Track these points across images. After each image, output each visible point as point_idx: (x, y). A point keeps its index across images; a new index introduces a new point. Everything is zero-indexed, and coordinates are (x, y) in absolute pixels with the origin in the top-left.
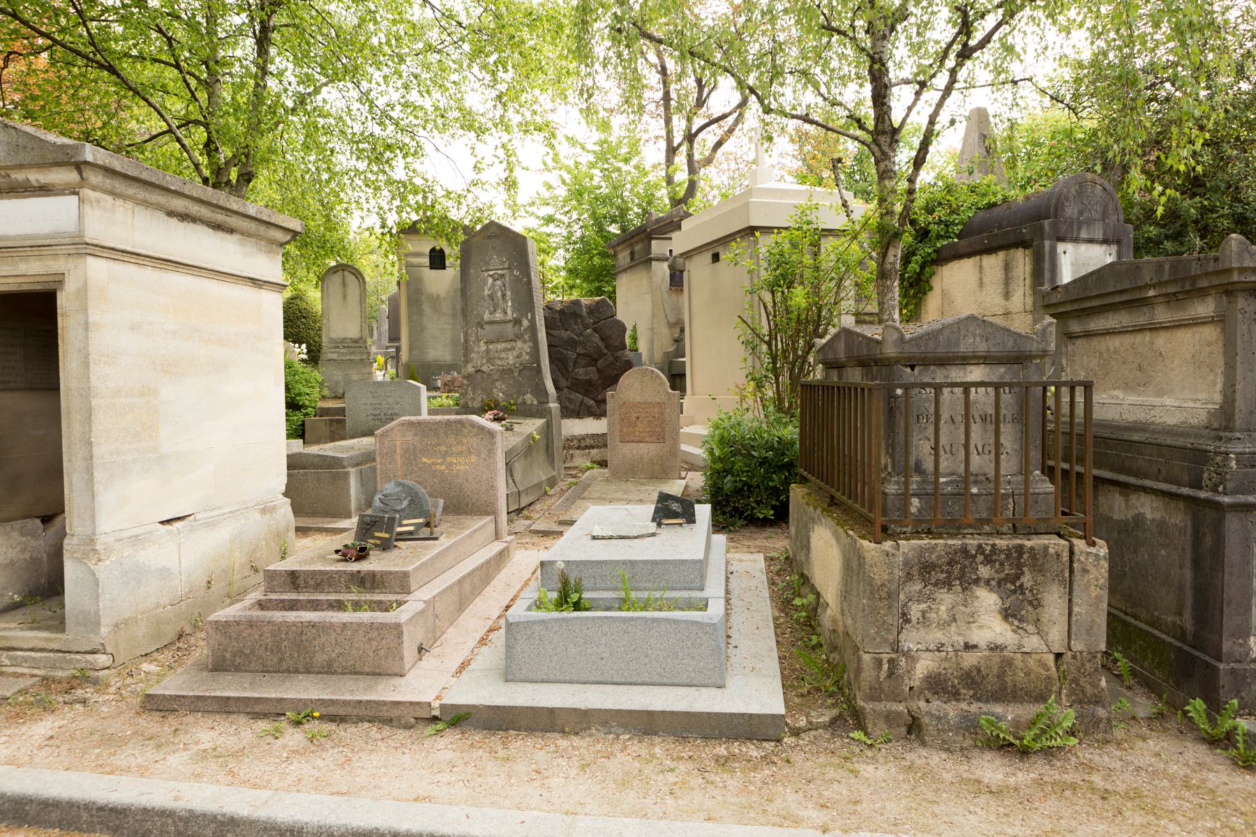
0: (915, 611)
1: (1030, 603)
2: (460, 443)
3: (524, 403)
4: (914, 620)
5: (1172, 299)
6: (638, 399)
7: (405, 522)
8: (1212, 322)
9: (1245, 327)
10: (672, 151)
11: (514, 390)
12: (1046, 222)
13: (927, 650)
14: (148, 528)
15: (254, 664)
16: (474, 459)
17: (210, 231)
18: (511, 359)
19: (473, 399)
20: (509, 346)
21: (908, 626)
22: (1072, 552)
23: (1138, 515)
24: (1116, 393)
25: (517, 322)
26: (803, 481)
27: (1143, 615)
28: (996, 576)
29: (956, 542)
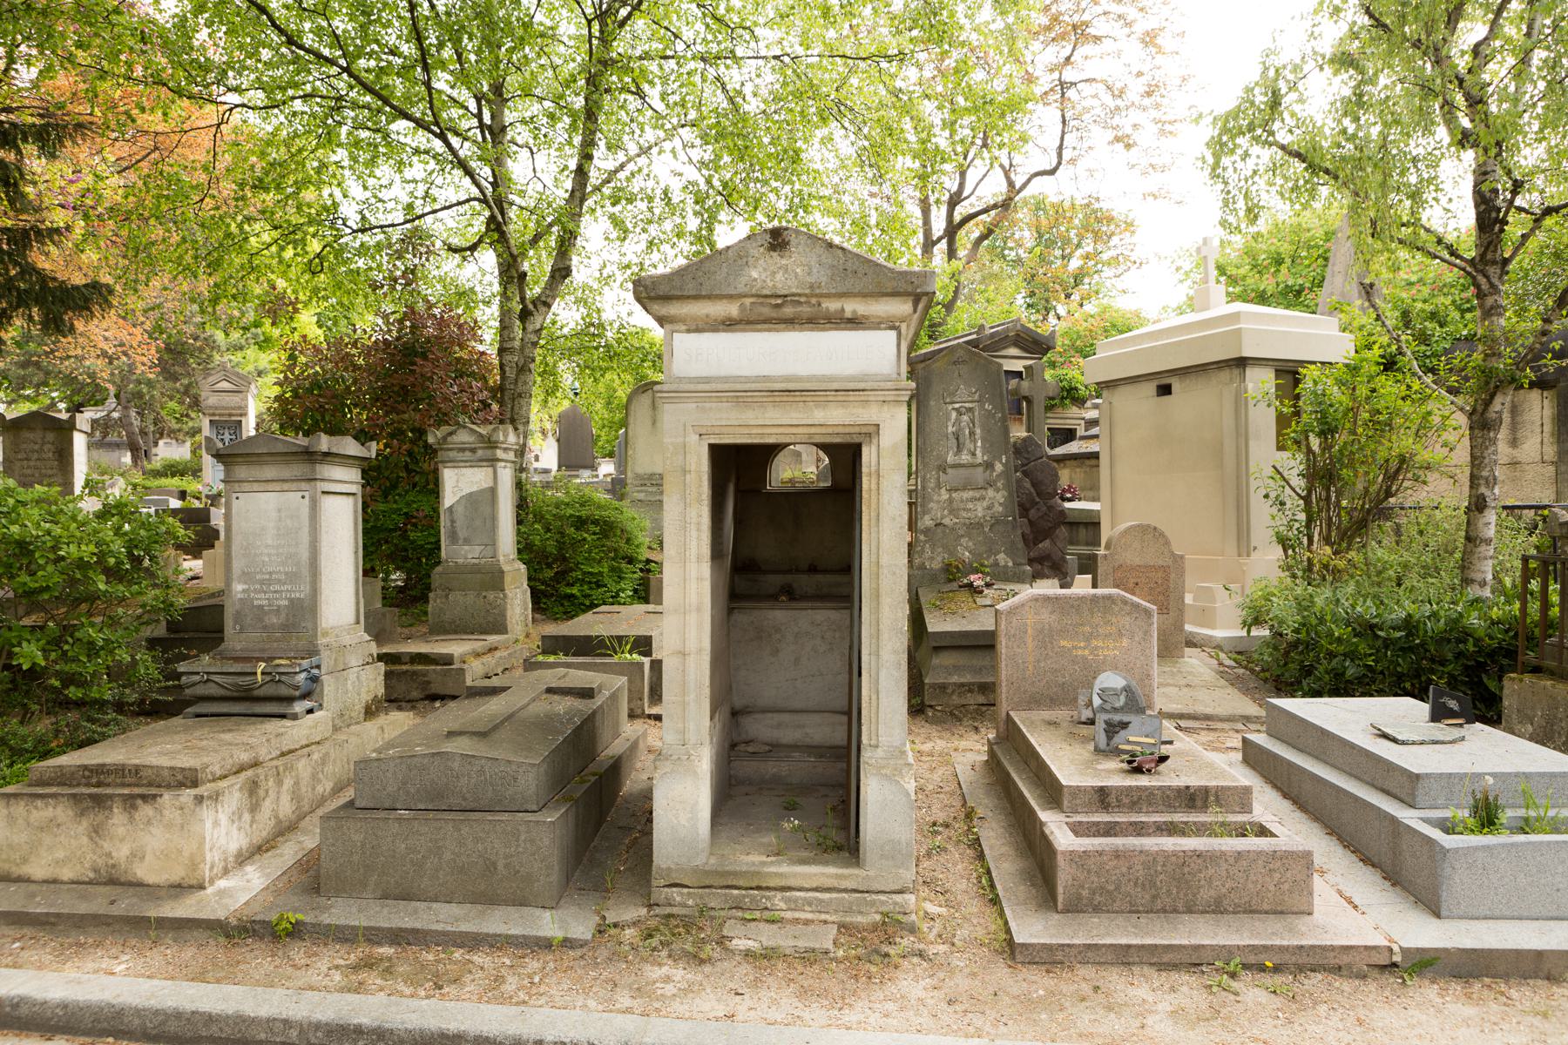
3: (996, 564)
6: (1137, 561)
15: (1118, 903)
16: (1125, 642)
18: (979, 510)
19: (932, 558)
20: (977, 494)
25: (989, 466)
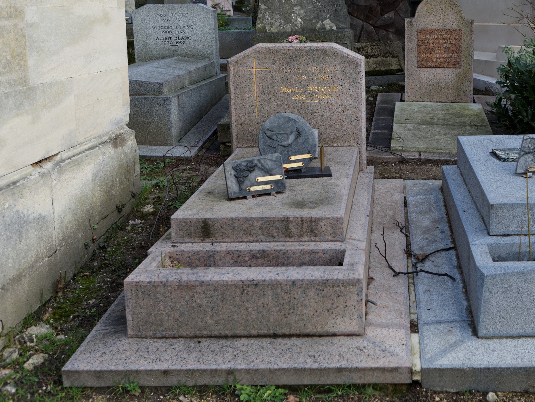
2: (322, 71)
7: (293, 158)
14: (24, 172)
16: (337, 88)
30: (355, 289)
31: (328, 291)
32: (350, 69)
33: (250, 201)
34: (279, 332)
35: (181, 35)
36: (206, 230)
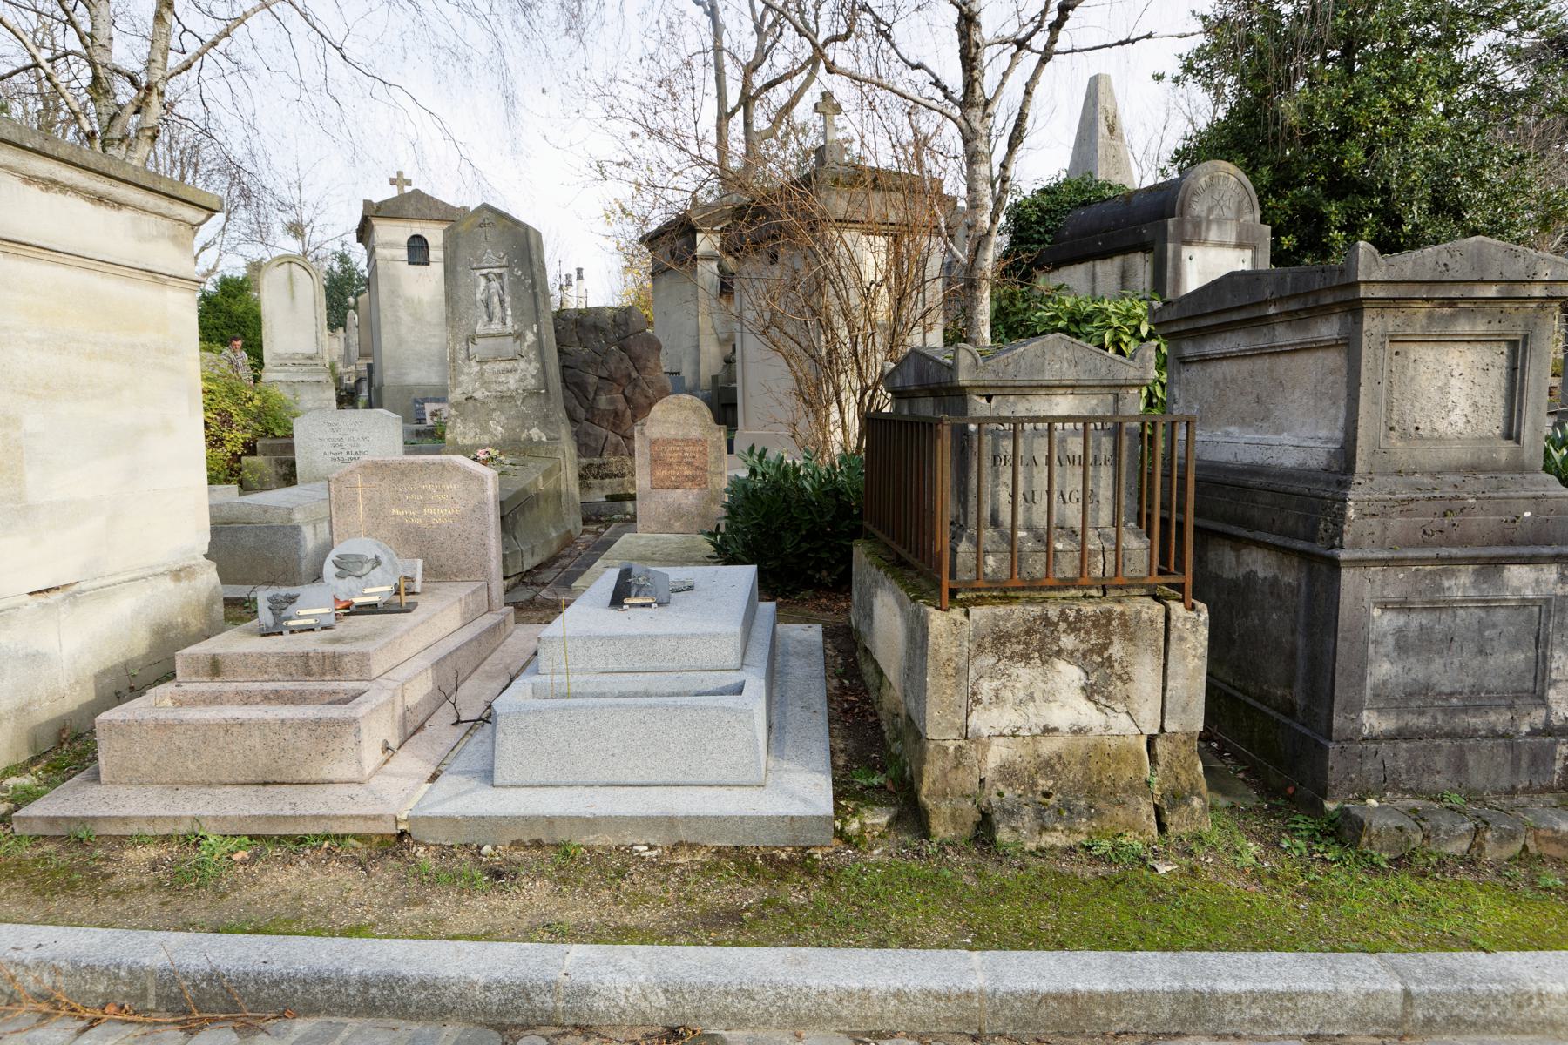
0: (986, 688)
1: (1120, 677)
2: (441, 490)
4: (985, 699)
5: (1292, 318)
7: (367, 591)
8: (1337, 345)
9: (1370, 352)
10: (724, 116)
11: (518, 423)
12: (1170, 221)
13: (1001, 735)
14: (14, 602)
17: (88, 205)
18: (512, 382)
20: (509, 365)
21: (979, 707)
22: (1167, 618)
23: (1249, 573)
24: (1232, 429)
25: (519, 336)
26: (870, 537)
27: (1252, 689)
28: (1082, 647)
29: (1036, 610)
30: (351, 730)
31: (322, 731)
32: (474, 487)
33: (287, 636)
34: (270, 779)
35: (354, 450)
36: (215, 667)
